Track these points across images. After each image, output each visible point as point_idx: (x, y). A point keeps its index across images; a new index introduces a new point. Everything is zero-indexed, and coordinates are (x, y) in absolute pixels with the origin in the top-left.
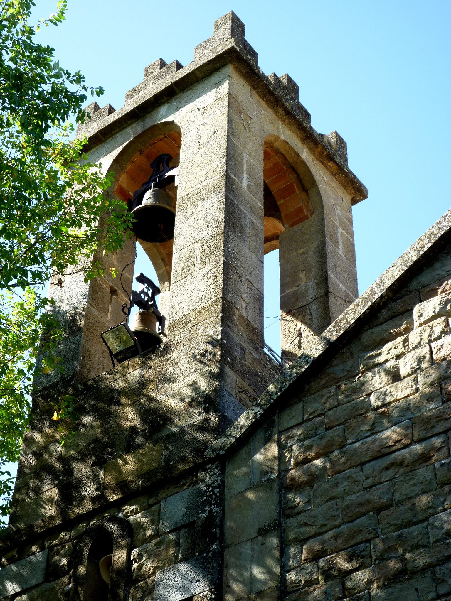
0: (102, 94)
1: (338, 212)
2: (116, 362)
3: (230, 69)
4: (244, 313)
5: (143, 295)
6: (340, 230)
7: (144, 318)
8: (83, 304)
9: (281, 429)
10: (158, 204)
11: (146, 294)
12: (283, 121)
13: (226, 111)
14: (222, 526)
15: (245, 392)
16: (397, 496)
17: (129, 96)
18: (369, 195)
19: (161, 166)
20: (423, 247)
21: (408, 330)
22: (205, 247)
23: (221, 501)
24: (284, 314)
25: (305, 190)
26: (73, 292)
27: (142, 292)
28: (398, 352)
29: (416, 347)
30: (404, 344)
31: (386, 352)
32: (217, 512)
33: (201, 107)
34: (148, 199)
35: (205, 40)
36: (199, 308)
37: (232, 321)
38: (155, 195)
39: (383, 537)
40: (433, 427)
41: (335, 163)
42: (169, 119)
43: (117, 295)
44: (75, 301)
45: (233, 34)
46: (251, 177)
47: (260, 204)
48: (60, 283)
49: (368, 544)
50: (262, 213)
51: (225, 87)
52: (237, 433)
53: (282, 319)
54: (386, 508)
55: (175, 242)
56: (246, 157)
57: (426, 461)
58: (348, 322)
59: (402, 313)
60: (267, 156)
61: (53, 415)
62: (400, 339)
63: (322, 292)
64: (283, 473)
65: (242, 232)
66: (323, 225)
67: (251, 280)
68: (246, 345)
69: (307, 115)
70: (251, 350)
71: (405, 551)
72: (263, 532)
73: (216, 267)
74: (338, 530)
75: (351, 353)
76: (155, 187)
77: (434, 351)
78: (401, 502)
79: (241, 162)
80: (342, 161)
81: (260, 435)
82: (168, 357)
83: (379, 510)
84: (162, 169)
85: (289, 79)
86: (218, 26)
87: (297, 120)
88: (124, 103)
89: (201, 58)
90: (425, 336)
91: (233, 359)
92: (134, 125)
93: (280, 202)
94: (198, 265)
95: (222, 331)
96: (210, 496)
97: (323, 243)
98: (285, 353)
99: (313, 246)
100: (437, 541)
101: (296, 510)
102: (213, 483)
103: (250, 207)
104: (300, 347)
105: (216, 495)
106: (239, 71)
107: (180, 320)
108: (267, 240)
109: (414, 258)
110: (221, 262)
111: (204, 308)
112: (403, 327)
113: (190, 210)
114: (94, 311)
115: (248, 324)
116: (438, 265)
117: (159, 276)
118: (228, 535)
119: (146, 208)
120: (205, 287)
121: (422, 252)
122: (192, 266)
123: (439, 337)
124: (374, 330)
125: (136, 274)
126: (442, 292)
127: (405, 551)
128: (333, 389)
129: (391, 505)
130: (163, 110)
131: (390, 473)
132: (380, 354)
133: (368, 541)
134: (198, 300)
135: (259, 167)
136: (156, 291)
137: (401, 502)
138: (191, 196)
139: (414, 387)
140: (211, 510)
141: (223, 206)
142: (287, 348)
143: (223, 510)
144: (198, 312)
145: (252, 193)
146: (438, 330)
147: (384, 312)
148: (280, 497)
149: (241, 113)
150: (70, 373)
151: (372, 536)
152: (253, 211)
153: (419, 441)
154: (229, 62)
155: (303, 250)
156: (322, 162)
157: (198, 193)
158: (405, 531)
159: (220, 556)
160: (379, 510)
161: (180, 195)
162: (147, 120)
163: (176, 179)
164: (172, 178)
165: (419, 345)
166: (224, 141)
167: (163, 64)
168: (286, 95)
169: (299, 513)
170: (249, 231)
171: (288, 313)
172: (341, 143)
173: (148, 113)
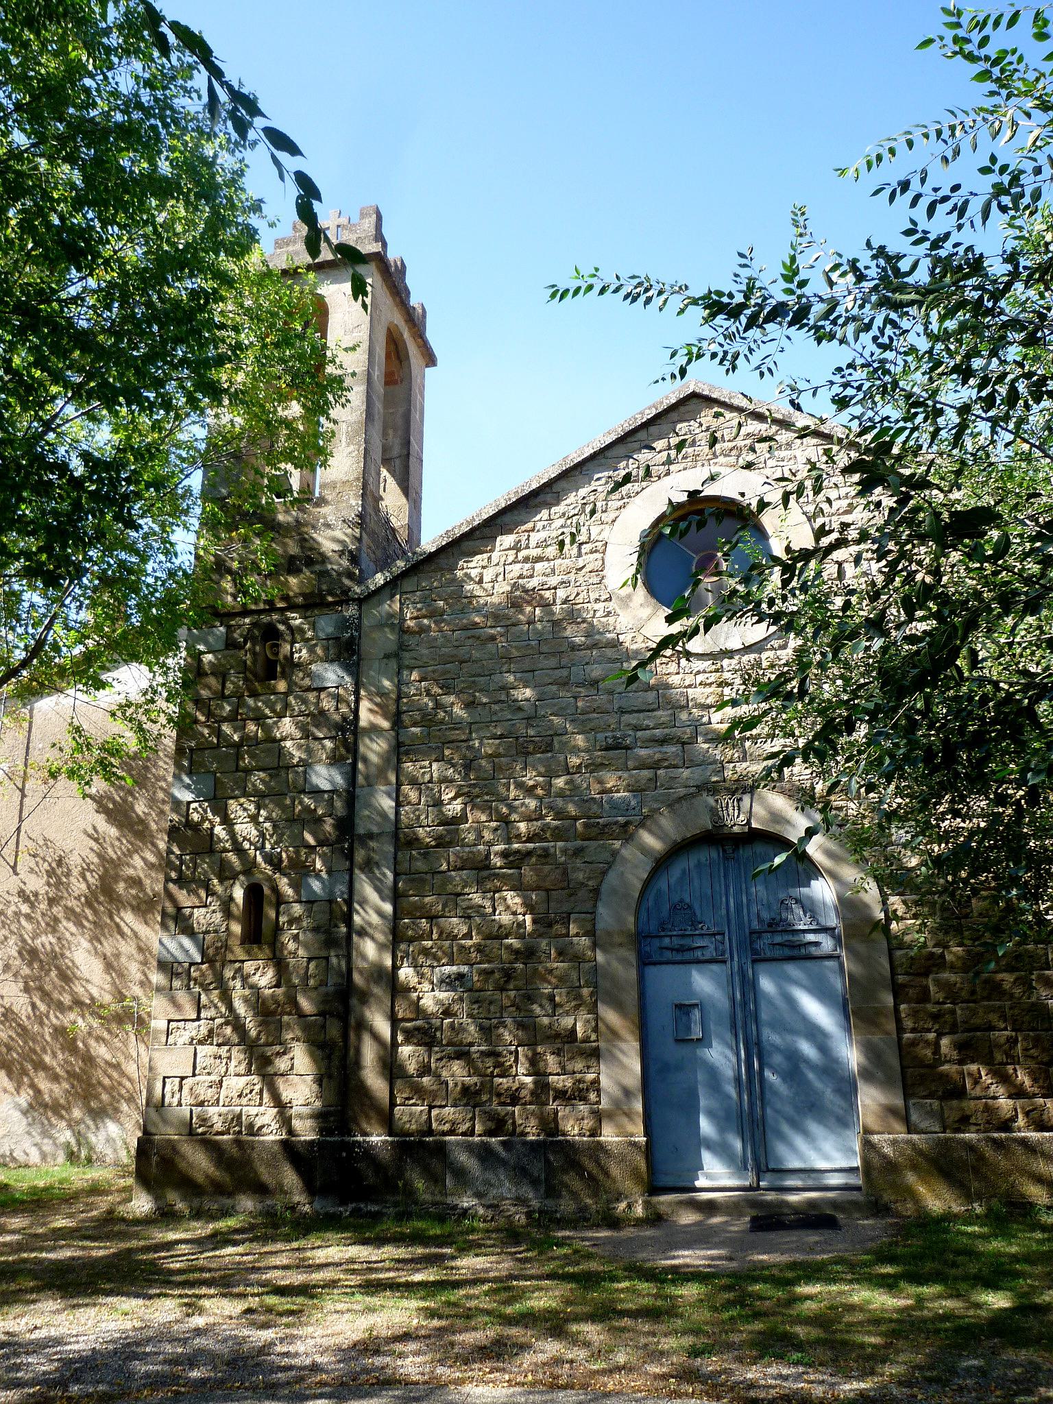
18: (439, 362)
21: (492, 551)
36: (345, 479)
52: (372, 588)
62: (485, 556)
81: (387, 591)
83: (461, 662)
90: (503, 559)
94: (344, 444)
97: (409, 411)
99: (401, 410)
106: (377, 267)
118: (362, 652)
146: (511, 559)
159: (358, 664)
160: (461, 662)
165: (497, 564)
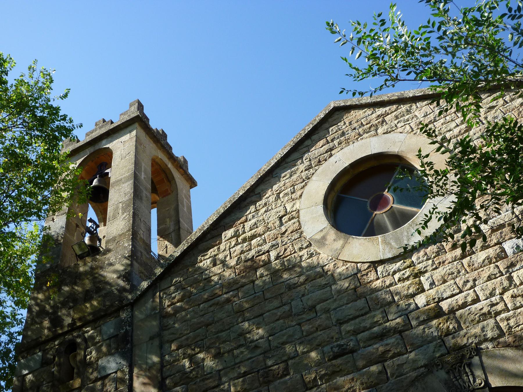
0: (82, 126)
1: (184, 191)
2: (79, 259)
3: (137, 125)
4: (142, 236)
5: (91, 228)
6: (185, 200)
7: (91, 239)
8: (62, 231)
9: (161, 290)
10: (101, 185)
11: (93, 228)
12: (160, 149)
13: (134, 143)
14: (132, 336)
15: (143, 273)
16: (216, 319)
17: (87, 135)
19: (102, 168)
20: (226, 206)
21: (220, 243)
22: (124, 205)
23: (131, 324)
24: (159, 237)
25: (169, 181)
26: (57, 226)
27: (91, 226)
28: (215, 253)
29: (224, 251)
30: (218, 250)
31: (210, 254)
32: (129, 329)
33: (123, 141)
34: (95, 182)
35: (125, 111)
37: (136, 239)
38: (99, 181)
39: (209, 338)
40: (232, 287)
41: (183, 170)
42: (107, 146)
43: (79, 227)
44: (57, 230)
45: (138, 110)
46: (145, 173)
47: (149, 187)
48: (53, 220)
49: (202, 341)
50: (150, 191)
51: (134, 133)
53: (158, 240)
54: (210, 324)
55: (109, 203)
56: (143, 165)
57: (229, 303)
58: (192, 240)
59: (217, 236)
60: (152, 165)
61: (47, 284)
62: (216, 248)
63: (177, 227)
64: (162, 310)
65: (141, 199)
66: (178, 197)
67: (145, 221)
68: (143, 251)
69: (171, 148)
70: (145, 253)
71: (220, 344)
72: (152, 338)
73: (129, 215)
74: (188, 336)
75: (194, 254)
76: (99, 177)
77: (232, 253)
78: (218, 321)
79: (141, 167)
80: (186, 169)
82: (105, 256)
83: (207, 325)
84: (102, 169)
85: (163, 132)
86: (131, 105)
87: (166, 150)
88: (85, 138)
89: (123, 119)
90: (228, 246)
91: (137, 257)
92: (89, 148)
93: (157, 187)
94: (120, 214)
95: (132, 244)
96: (126, 322)
97: (177, 206)
98: (159, 255)
99: (173, 207)
100: (234, 339)
101: (168, 327)
102: (128, 316)
103: (145, 188)
104: (167, 253)
105: (129, 321)
106: (141, 126)
107: (111, 239)
108: (152, 203)
109: (222, 211)
110: (132, 212)
111: (123, 233)
112: (218, 242)
113: (117, 188)
114: (68, 235)
115: (144, 241)
116: (233, 214)
117: (98, 219)
119: (95, 187)
120: (124, 223)
121: (226, 209)
122: (117, 214)
123: (234, 247)
124: (204, 243)
125: (88, 219)
126: (235, 227)
127: (220, 344)
128: (185, 270)
129: (213, 323)
130: (104, 142)
131: (212, 309)
132: (207, 254)
133: (202, 340)
134: (120, 230)
135: (149, 169)
136: (98, 226)
137: (218, 321)
138: (114, 183)
139: (223, 269)
140: (127, 329)
141: (133, 187)
142: (161, 253)
143: (132, 329)
144: (120, 235)
145: (146, 181)
146: (233, 243)
147: (209, 235)
148: (160, 321)
149: (141, 145)
150: (55, 265)
151: (204, 337)
152: (146, 189)
153: (226, 293)
154: (136, 122)
155: (168, 208)
156: (177, 169)
157: (121, 180)
158: (220, 334)
159: (131, 350)
160: (207, 325)
161: (112, 181)
162: (96, 146)
163: (110, 174)
164: (108, 173)
165: (225, 250)
166: (133, 157)
167: (104, 121)
168: (162, 138)
169: (169, 329)
170: (144, 198)
171: (161, 237)
172: (185, 161)
173: (97, 143)
